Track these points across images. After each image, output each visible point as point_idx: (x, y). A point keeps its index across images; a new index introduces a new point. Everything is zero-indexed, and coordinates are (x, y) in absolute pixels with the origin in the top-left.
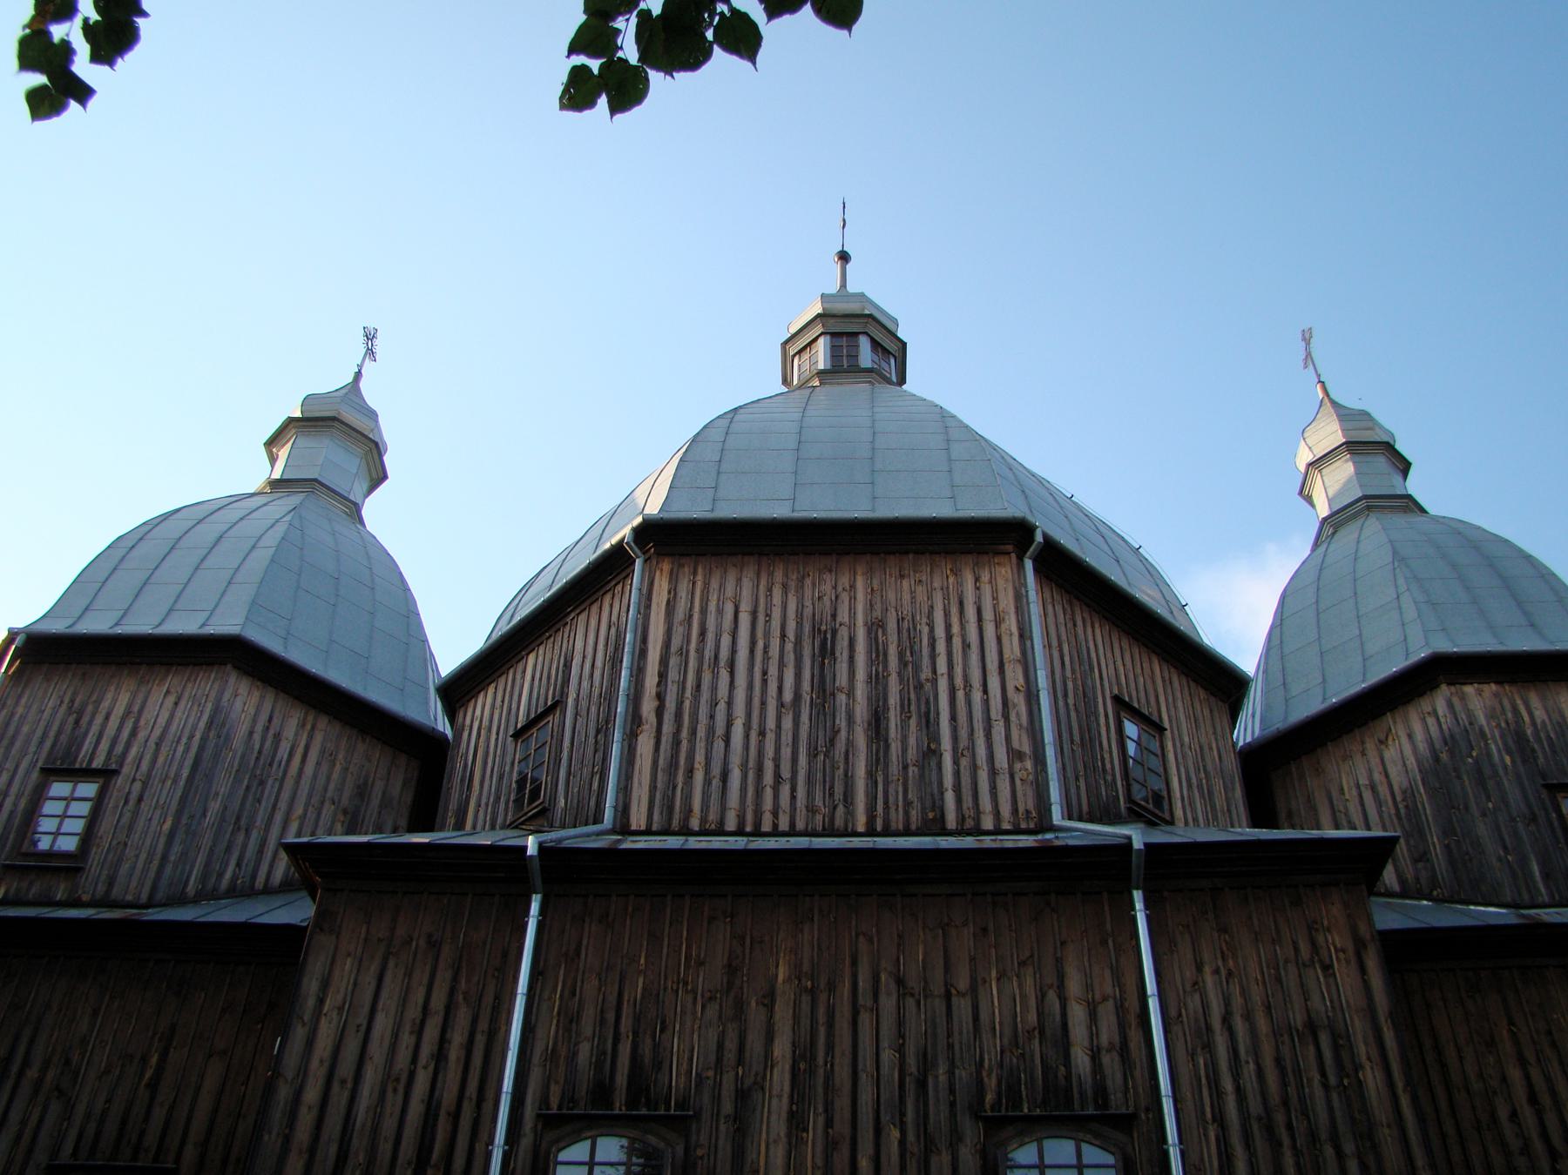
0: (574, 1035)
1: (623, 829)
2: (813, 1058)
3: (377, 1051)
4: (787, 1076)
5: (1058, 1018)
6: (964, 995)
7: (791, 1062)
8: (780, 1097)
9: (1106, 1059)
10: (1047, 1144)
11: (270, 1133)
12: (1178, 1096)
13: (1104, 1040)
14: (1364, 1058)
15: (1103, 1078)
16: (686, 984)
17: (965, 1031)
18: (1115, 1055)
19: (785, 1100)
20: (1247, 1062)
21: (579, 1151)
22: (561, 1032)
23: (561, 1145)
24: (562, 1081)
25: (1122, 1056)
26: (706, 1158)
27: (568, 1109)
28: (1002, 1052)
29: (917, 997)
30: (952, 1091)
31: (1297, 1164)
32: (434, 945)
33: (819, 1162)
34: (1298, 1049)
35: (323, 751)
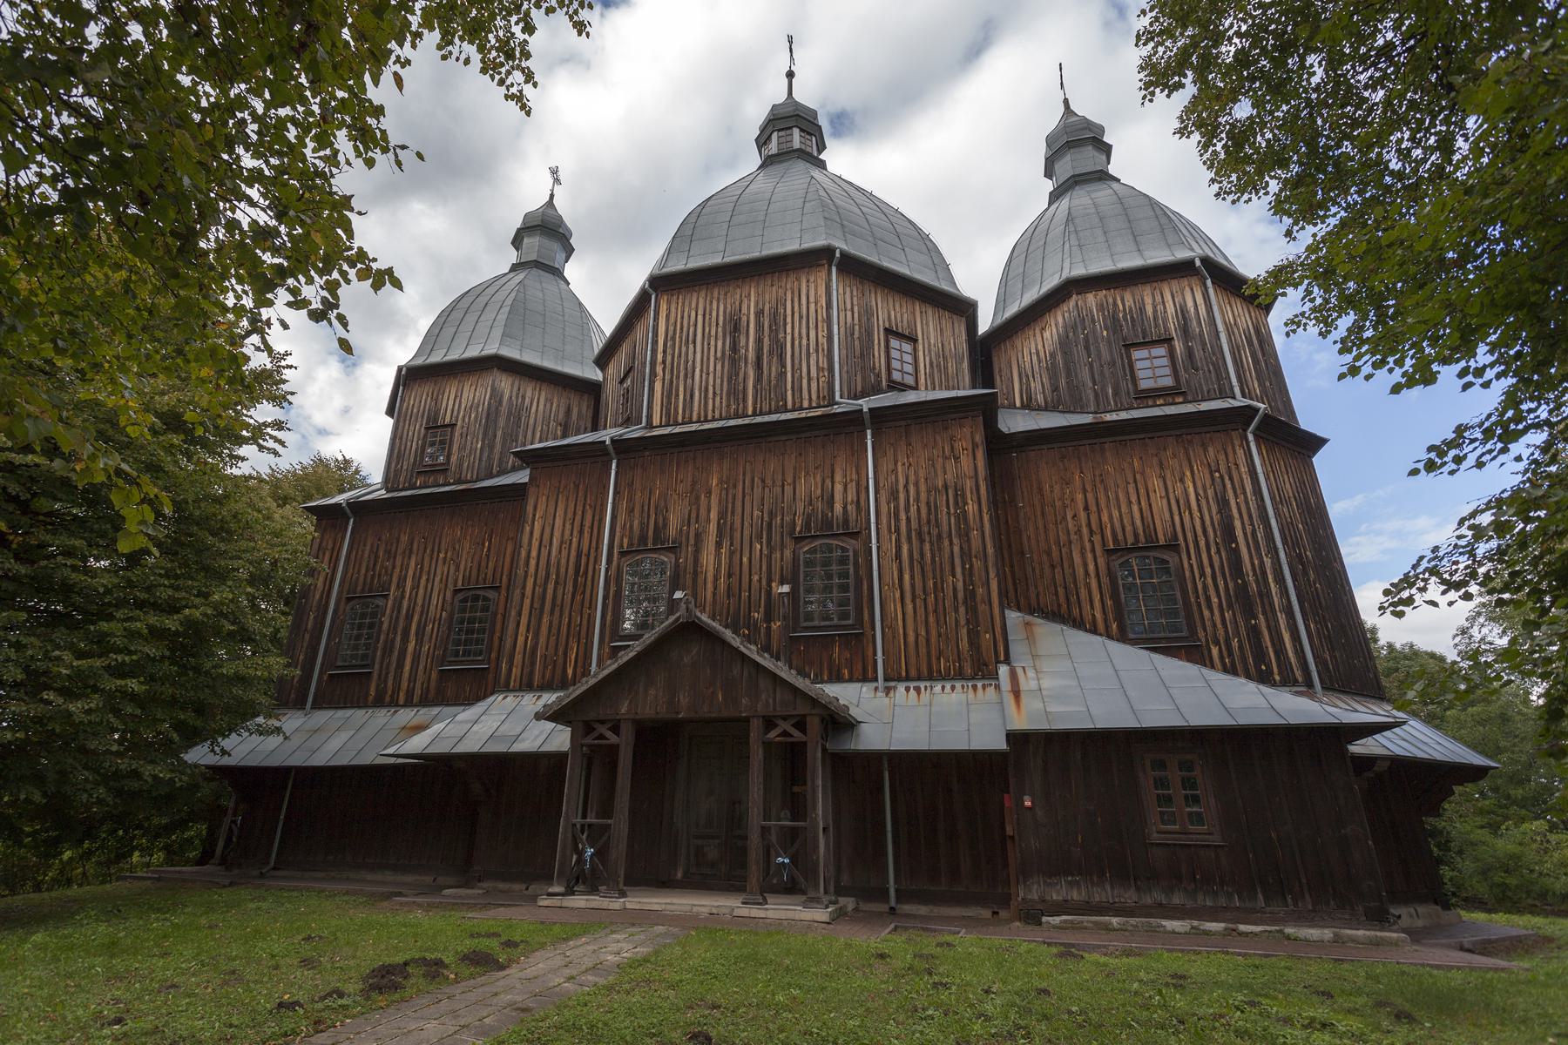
1: (650, 426)
9: (849, 507)
32: (577, 486)
35: (546, 399)
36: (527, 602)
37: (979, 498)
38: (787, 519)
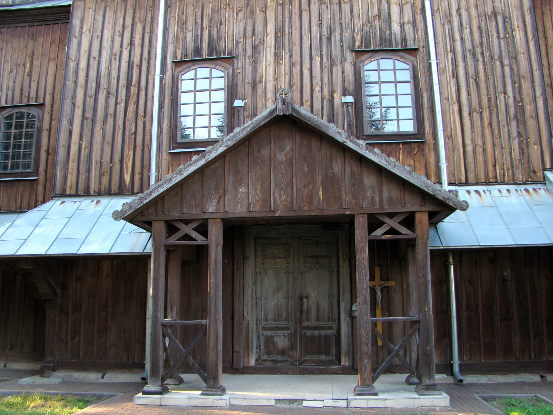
0: (184, 30)
2: (284, 31)
3: (106, 44)
4: (273, 39)
5: (387, 11)
6: (347, 3)
7: (274, 33)
8: (270, 47)
9: (406, 27)
10: (381, 61)
11: (69, 81)
12: (436, 42)
13: (406, 20)
14: (516, 26)
15: (405, 35)
16: (229, 5)
17: (347, 18)
18: (410, 25)
19: (273, 48)
20: (466, 28)
21: (190, 74)
22: (179, 29)
23: (183, 73)
24: (181, 48)
25: (413, 26)
26: (241, 73)
27: (184, 59)
28: (363, 25)
29: (327, 4)
30: (342, 42)
31: (484, 68)
33: (288, 72)
34: (488, 23)
36: (78, 112)
37: (525, 26)
38: (347, 35)
